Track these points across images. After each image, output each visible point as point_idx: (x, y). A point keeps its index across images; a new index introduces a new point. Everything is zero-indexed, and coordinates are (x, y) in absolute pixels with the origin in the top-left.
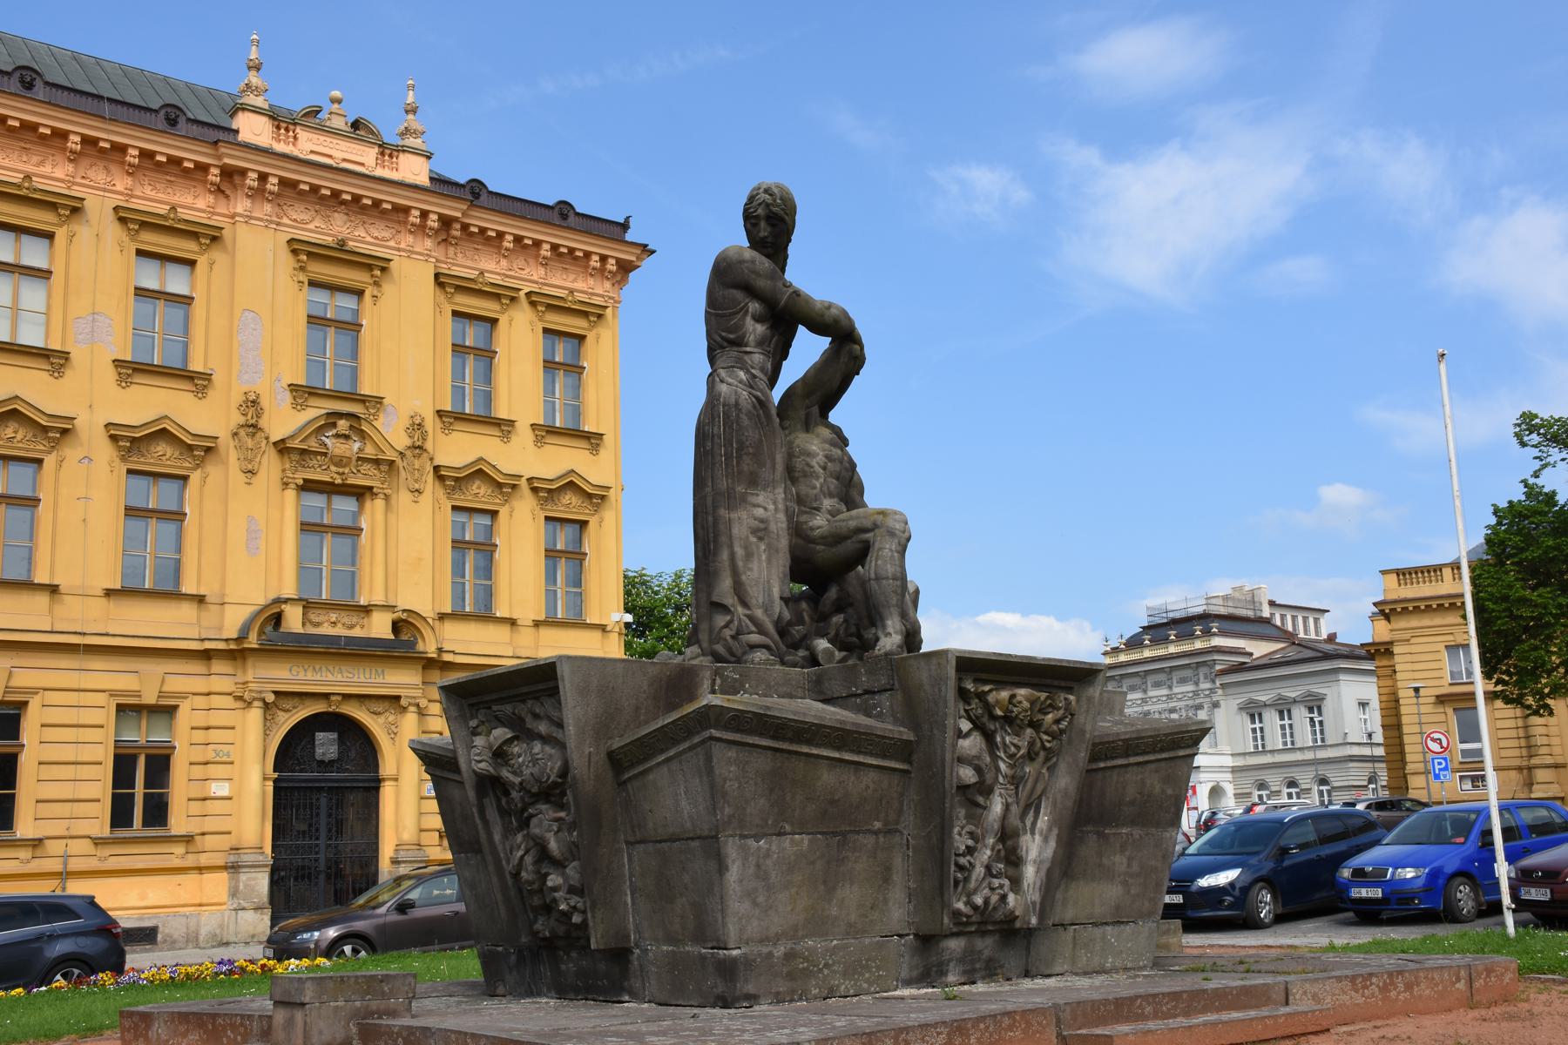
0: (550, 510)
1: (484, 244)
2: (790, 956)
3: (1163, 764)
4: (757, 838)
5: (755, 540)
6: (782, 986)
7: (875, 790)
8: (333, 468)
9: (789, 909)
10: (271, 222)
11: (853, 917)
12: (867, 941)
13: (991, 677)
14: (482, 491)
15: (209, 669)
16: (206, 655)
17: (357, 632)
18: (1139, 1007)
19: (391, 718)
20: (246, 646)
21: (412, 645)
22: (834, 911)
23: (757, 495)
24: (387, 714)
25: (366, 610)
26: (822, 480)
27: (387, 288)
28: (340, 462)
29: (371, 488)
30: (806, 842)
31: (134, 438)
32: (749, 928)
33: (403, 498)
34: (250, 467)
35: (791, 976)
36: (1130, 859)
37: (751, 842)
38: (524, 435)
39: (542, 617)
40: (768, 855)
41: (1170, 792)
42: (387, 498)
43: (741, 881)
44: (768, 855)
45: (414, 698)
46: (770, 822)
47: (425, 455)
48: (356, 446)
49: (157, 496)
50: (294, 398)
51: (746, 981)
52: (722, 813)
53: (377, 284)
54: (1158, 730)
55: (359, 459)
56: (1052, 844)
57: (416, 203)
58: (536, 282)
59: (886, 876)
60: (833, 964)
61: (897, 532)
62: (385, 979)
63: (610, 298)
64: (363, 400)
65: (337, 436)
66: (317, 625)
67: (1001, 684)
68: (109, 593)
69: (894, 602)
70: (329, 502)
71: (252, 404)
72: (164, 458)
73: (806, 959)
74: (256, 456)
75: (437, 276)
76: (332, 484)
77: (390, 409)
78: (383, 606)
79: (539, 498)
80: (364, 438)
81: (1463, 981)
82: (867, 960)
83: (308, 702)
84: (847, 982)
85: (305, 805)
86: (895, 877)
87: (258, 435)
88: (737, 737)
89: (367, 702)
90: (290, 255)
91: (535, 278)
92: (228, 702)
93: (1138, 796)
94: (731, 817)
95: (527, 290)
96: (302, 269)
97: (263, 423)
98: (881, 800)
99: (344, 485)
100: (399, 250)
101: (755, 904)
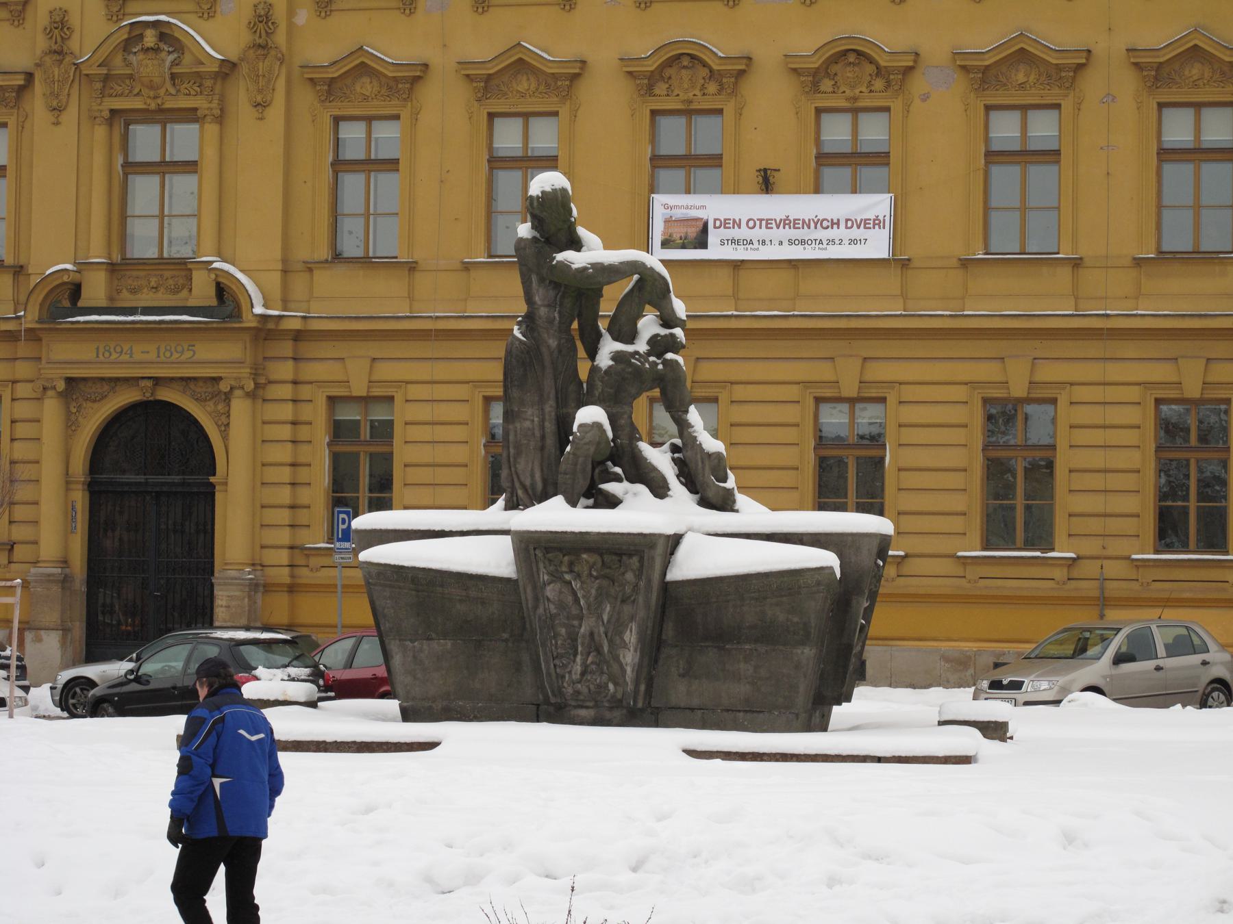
9: (441, 682)
23: (527, 412)
41: (796, 619)
46: (420, 632)
72: (1200, 83)
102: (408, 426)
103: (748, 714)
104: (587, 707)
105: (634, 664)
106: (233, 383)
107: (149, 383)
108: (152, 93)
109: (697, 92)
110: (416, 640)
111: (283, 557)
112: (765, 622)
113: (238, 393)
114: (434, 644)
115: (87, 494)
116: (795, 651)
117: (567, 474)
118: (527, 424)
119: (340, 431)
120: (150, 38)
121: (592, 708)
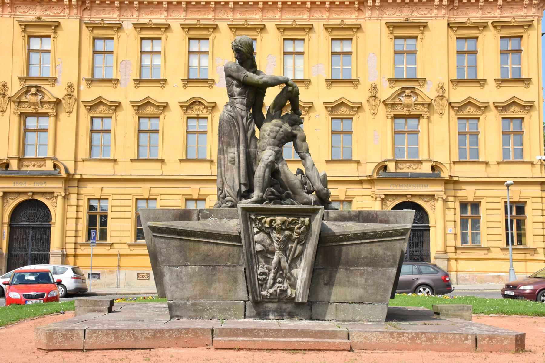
0: (504, 115)
1: (471, 6)
2: (193, 305)
3: (384, 243)
4: (176, 266)
5: (230, 164)
6: (192, 314)
7: (226, 252)
8: (405, 109)
10: (379, 17)
11: (221, 294)
12: (228, 302)
13: (262, 213)
14: (472, 110)
15: (362, 187)
16: (361, 182)
17: (418, 171)
18: (256, 332)
19: (432, 203)
20: (372, 178)
21: (439, 175)
22: (212, 291)
24: (431, 202)
25: (421, 162)
26: (268, 140)
27: (426, 33)
28: (408, 106)
29: (421, 115)
31: (333, 107)
32: (176, 295)
33: (435, 117)
34: (374, 112)
35: (195, 311)
36: (366, 280)
37: (174, 268)
38: (491, 83)
39: (501, 160)
40: (181, 272)
41: (389, 253)
42: (428, 118)
43: (170, 280)
44: (181, 272)
45: (441, 195)
47: (445, 99)
48: (414, 99)
49: (341, 126)
50: (390, 84)
51: (176, 311)
53: (422, 33)
54: (376, 230)
55: (415, 104)
56: (306, 272)
58: (497, 17)
59: (235, 280)
60: (214, 308)
61: (264, 160)
62: (100, 301)
63: (535, 16)
64: (417, 80)
65: (406, 96)
66: (402, 169)
67: (268, 216)
68: (327, 162)
70: (406, 122)
73: (201, 306)
74: (376, 108)
75: (448, 24)
76: (405, 115)
77: (429, 82)
78: (427, 160)
79: (498, 110)
80: (417, 96)
81: (470, 341)
82: (229, 308)
83: (399, 198)
85: (415, 235)
86: (239, 281)
87: (376, 100)
88: (164, 235)
89: (422, 197)
90: (387, 28)
91: (496, 15)
92: (369, 198)
93: (369, 255)
94: (164, 260)
95: (491, 21)
96: (392, 33)
97: (377, 95)
98: (230, 255)
99: (410, 115)
100: (431, 17)
101: (177, 287)
102: (286, 41)
103: (361, 305)
104: (273, 302)
106: (58, 194)
107: (31, 194)
108: (34, 107)
109: (200, 112)
111: (73, 246)
112: (372, 255)
113: (59, 197)
114: (189, 268)
115: (9, 228)
116: (387, 270)
118: (232, 155)
119: (91, 208)
120: (33, 90)
121: (276, 302)
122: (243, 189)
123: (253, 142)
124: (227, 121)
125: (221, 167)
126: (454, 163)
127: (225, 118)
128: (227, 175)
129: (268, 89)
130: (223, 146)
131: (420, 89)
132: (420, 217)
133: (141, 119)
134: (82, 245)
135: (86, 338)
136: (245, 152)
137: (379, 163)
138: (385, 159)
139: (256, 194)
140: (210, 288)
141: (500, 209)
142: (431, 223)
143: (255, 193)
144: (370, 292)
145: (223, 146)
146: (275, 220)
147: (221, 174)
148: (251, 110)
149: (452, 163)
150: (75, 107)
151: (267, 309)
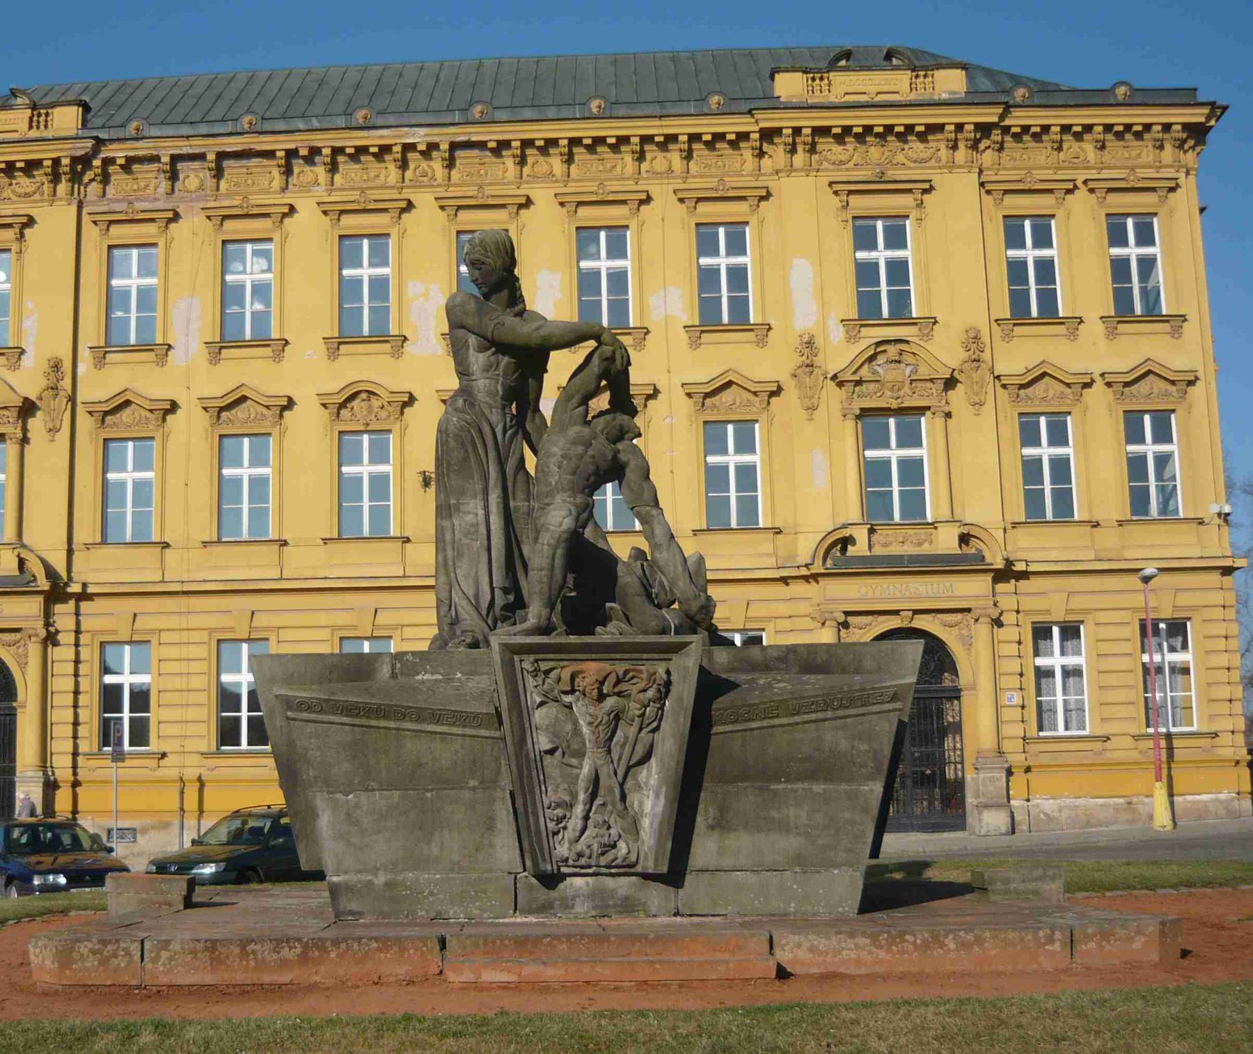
2: (389, 885)
4: (346, 794)
11: (456, 857)
23: (468, 504)
26: (557, 478)
30: (396, 796)
37: (338, 796)
40: (357, 806)
41: (864, 747)
52: (308, 774)
56: (662, 800)
57: (948, 117)
61: (552, 527)
69: (537, 590)
71: (809, 344)
75: (982, 184)
84: (456, 908)
86: (499, 825)
97: (818, 360)
98: (474, 762)
101: (349, 843)
105: (655, 815)
110: (350, 793)
117: (541, 570)
118: (470, 518)
122: (500, 601)
123: (521, 484)
124: (456, 435)
125: (444, 549)
126: (1015, 525)
127: (451, 428)
128: (460, 567)
129: (552, 354)
130: (447, 496)
131: (922, 343)
132: (935, 667)
133: (225, 440)
134: (89, 755)
135: (146, 960)
136: (502, 510)
137: (829, 533)
138: (845, 522)
139: (535, 612)
140: (429, 842)
141: (1134, 703)
142: (964, 679)
143: (531, 609)
144: (820, 842)
145: (447, 496)
146: (581, 672)
147: (446, 566)
148: (514, 405)
149: (1009, 526)
150: (68, 414)
151: (570, 892)
